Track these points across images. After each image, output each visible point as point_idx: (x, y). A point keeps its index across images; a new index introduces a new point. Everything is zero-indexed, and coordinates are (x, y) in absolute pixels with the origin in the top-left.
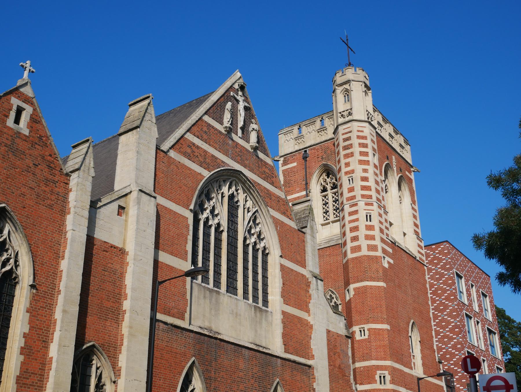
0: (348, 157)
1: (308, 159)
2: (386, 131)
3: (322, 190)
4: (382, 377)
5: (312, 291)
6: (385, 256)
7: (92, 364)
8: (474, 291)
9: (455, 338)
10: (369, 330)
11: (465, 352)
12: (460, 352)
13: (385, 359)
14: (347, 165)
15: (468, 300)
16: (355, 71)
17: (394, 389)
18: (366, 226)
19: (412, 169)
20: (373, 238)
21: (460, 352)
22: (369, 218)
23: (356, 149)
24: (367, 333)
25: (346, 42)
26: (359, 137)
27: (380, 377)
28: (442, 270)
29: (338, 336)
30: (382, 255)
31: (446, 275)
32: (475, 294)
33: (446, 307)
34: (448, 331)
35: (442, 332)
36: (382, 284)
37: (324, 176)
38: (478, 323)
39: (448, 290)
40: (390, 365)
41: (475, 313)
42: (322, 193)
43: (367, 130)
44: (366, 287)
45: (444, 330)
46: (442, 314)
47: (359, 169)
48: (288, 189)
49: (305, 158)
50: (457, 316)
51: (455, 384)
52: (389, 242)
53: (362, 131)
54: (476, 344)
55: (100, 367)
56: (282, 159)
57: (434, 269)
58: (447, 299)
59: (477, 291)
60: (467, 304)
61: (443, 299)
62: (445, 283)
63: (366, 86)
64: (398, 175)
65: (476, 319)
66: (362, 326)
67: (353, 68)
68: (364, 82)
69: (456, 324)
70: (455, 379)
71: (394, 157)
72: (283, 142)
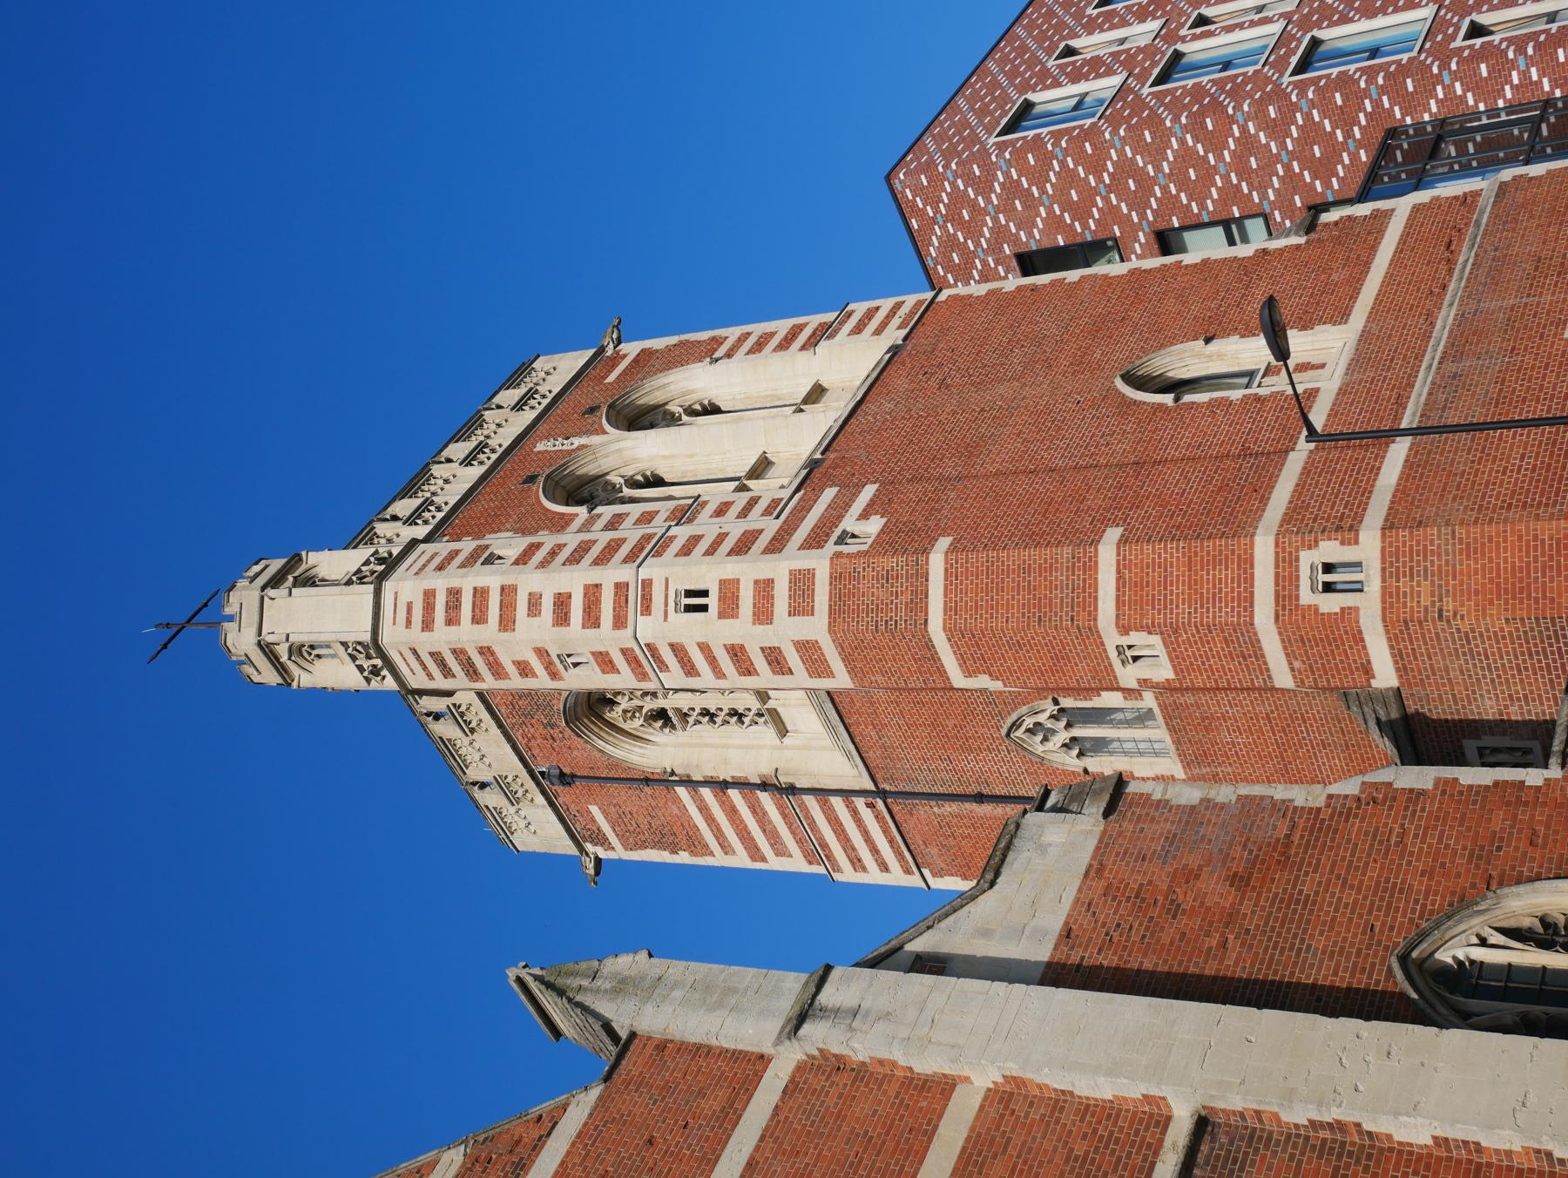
0: (499, 664)
1: (567, 770)
2: (453, 479)
3: (665, 725)
4: (1329, 578)
5: (862, 1047)
6: (838, 532)
7: (1460, 963)
8: (1090, 44)
9: (1244, 130)
10: (1124, 630)
11: (1296, 85)
12: (1295, 107)
13: (1248, 562)
14: (524, 669)
15: (1110, 72)
16: (231, 618)
17: (1380, 522)
18: (721, 615)
19: (609, 351)
20: (764, 588)
21: (1295, 107)
23: (467, 634)
24: (1136, 638)
25: (175, 629)
26: (427, 625)
27: (1328, 588)
28: (992, 190)
29: (1100, 871)
30: (831, 547)
31: (1007, 175)
32: (1098, 38)
33: (1126, 168)
34: (1220, 158)
35: (1226, 178)
36: (936, 562)
37: (614, 714)
38: (1202, 21)
39: (1063, 164)
40: (1271, 540)
41: (1164, 39)
42: (673, 727)
43: (404, 587)
44: (950, 630)
45: (1215, 169)
46: (1154, 180)
47: (534, 631)
48: (681, 837)
49: (565, 779)
50: (1155, 122)
51: (1427, 117)
52: (798, 496)
54: (1276, 28)
55: (1478, 936)
56: (589, 847)
57: (995, 220)
58: (1096, 167)
59: (1091, 27)
60: (1125, 74)
61: (1100, 180)
62: (1039, 178)
63: (276, 581)
64: (605, 432)
65: (1183, 32)
66: (1113, 654)
67: (225, 624)
68: (263, 589)
69: (1185, 129)
70: (1409, 120)
71: (540, 447)
72: (532, 837)
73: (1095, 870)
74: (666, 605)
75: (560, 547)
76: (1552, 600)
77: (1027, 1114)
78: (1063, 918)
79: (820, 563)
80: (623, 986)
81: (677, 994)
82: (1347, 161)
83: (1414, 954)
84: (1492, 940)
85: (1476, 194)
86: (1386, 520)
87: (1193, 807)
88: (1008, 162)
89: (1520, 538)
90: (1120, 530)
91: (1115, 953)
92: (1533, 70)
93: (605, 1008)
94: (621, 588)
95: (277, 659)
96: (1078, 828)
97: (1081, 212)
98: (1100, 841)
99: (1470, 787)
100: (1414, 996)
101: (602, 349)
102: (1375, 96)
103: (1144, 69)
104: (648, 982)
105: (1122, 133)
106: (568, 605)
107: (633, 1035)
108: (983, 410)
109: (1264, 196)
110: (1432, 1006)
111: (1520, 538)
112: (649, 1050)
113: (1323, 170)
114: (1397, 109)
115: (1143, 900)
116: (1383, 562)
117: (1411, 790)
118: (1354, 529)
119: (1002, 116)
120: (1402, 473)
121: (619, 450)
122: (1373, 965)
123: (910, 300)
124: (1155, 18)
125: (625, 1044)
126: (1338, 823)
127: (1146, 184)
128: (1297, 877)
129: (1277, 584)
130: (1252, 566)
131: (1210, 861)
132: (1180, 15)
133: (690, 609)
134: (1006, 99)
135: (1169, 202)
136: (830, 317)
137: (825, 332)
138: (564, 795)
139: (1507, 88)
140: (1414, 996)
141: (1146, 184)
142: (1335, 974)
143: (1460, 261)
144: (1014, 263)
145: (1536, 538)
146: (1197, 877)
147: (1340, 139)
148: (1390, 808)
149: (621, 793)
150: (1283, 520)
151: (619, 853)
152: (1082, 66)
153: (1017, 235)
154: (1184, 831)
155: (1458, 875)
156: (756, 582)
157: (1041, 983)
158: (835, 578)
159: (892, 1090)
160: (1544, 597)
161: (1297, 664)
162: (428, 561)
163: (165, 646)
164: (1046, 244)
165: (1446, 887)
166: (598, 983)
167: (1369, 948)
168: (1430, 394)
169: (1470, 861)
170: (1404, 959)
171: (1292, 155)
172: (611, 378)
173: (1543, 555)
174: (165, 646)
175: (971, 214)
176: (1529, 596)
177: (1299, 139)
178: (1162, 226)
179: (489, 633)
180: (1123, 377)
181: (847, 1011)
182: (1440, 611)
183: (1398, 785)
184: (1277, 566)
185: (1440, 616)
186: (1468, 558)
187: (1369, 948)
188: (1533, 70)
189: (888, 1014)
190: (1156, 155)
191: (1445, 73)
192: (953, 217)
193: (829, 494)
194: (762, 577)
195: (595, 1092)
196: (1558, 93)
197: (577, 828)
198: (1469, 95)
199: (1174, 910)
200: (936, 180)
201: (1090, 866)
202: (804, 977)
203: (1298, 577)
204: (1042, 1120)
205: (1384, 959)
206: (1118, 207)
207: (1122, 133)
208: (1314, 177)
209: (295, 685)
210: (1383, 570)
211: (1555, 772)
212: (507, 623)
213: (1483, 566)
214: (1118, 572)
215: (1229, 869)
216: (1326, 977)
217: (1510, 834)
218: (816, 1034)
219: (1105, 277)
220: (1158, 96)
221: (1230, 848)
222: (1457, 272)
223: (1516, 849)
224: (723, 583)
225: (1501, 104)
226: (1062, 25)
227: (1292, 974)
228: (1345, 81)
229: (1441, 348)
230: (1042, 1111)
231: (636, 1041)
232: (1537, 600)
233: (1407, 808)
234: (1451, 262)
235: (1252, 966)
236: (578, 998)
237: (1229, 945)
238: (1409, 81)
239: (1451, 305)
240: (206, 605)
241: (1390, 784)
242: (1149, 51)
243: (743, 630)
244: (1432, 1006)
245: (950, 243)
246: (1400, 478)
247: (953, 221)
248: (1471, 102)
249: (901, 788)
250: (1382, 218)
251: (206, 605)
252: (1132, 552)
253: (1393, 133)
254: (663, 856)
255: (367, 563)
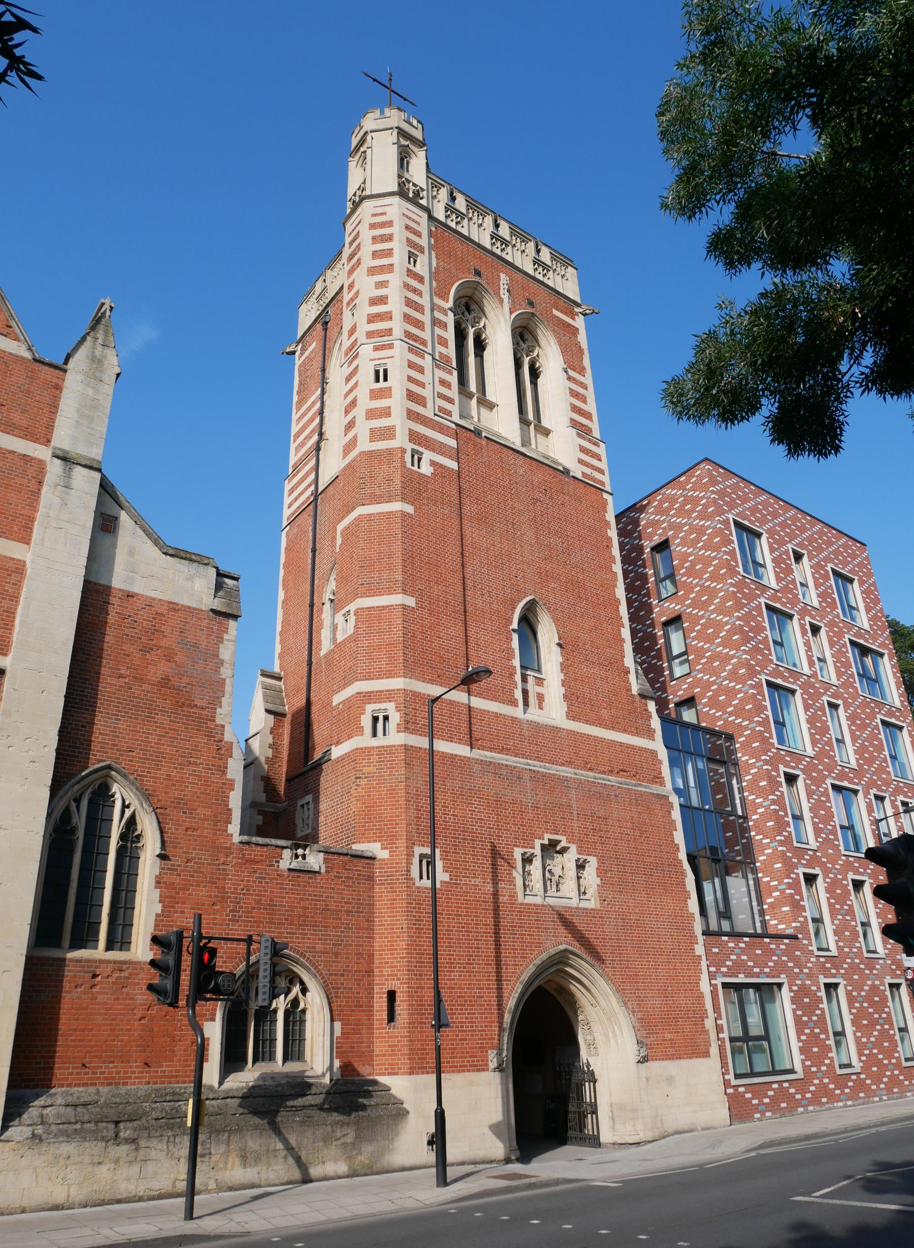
5: (48, 495)
7: (113, 796)
12: (744, 683)
13: (390, 675)
16: (382, 113)
18: (372, 391)
19: (577, 310)
22: (381, 375)
24: (352, 619)
25: (387, 84)
26: (373, 226)
27: (375, 719)
30: (409, 446)
35: (708, 650)
36: (396, 506)
38: (815, 630)
39: (715, 558)
40: (401, 686)
44: (358, 519)
50: (739, 606)
52: (453, 426)
53: (384, 214)
54: (806, 670)
55: (130, 804)
56: (300, 346)
62: (708, 546)
63: (402, 133)
64: (511, 313)
65: (808, 619)
66: (347, 609)
70: (738, 746)
71: (502, 276)
73: (173, 607)
74: (379, 359)
75: (420, 294)
76: (364, 834)
77: (9, 583)
78: (141, 593)
79: (400, 441)
80: (97, 362)
81: (90, 392)
82: (717, 714)
83: (113, 773)
84: (127, 810)
85: (662, 783)
86: (412, 747)
87: (218, 656)
88: (715, 527)
89: (397, 816)
90: (414, 605)
91: (116, 621)
92: (763, 810)
93: (82, 354)
94: (389, 332)
95: (361, 145)
96: (204, 597)
97: (690, 572)
98: (194, 609)
99: (228, 797)
100: (83, 774)
101: (579, 305)
102: (750, 726)
103: (780, 598)
104: (98, 374)
105: (731, 589)
106: (381, 304)
107: (65, 371)
108: (514, 524)
109: (699, 671)
110: (78, 782)
111: (397, 816)
112: (55, 380)
113: (714, 703)
114: (744, 739)
115: (153, 634)
116: (387, 747)
117: (226, 768)
118: (406, 729)
119: (750, 521)
120: (447, 754)
121: (499, 322)
122: (107, 753)
123: (606, 478)
124: (820, 603)
125: (61, 369)
126: (205, 731)
127: (704, 606)
128: (167, 712)
129: (377, 692)
130: (387, 678)
131: (179, 666)
132: (821, 616)
133: (377, 373)
134: (763, 521)
135: (695, 620)
136: (596, 434)
137: (583, 431)
138: (319, 326)
139: (754, 797)
140: (83, 774)
141: (704, 606)
142: (100, 734)
143: (610, 777)
144: (664, 538)
145: (398, 824)
146: (169, 661)
147: (729, 710)
148: (213, 757)
149: (319, 359)
150: (415, 692)
151: (298, 363)
152: (786, 564)
153: (678, 537)
154: (201, 652)
155: (166, 793)
156: (389, 407)
157: (85, 581)
158: (390, 451)
159: (26, 512)
160: (365, 830)
161: (341, 706)
162: (413, 220)
163: (375, 80)
164: (674, 554)
165: (159, 787)
166: (100, 348)
167: (117, 750)
168: (507, 766)
169: (175, 798)
170: (109, 767)
171: (720, 684)
172: (555, 312)
173: (388, 828)
174: (375, 80)
175: (688, 510)
176: (366, 822)
177: (728, 687)
178: (684, 618)
179: (368, 262)
180: (534, 600)
181: (68, 482)
182: (360, 778)
183: (230, 760)
184: (387, 691)
185: (357, 778)
186: (388, 790)
187: (117, 750)
188: (763, 810)
189: (66, 504)
190: (720, 610)
191: (762, 763)
192: (687, 500)
193: (453, 443)
194: (392, 410)
195: (27, 355)
196: (751, 823)
197: (307, 338)
198: (750, 777)
199: (145, 650)
200: (705, 487)
201: (178, 605)
202: (99, 458)
203: (380, 702)
204: (4, 590)
205: (110, 757)
206: (693, 592)
207: (731, 589)
208: (710, 698)
209: (351, 159)
210: (383, 747)
211: (236, 838)
212: (372, 271)
213: (383, 798)
214: (387, 606)
215: (173, 677)
216: (99, 729)
217: (195, 818)
218: (55, 468)
219: (615, 586)
220: (759, 606)
221: (188, 676)
222: (600, 776)
223: (185, 821)
224: (390, 389)
225: (746, 794)
226: (820, 550)
227: (102, 712)
228: (760, 709)
229: (542, 770)
230: (10, 590)
231: (61, 373)
232: (364, 826)
233: (214, 765)
234: (611, 772)
235: (106, 692)
236: (89, 338)
237: (121, 679)
238: (758, 744)
239: (576, 774)
240: (405, 100)
241: (231, 757)
242: (795, 600)
243: (365, 403)
244: (78, 782)
245: (673, 500)
246: (443, 753)
247: (684, 500)
248: (747, 778)
249: (319, 508)
250: (650, 734)
251: (405, 100)
252: (398, 613)
253: (730, 738)
254: (296, 389)
255: (414, 185)
